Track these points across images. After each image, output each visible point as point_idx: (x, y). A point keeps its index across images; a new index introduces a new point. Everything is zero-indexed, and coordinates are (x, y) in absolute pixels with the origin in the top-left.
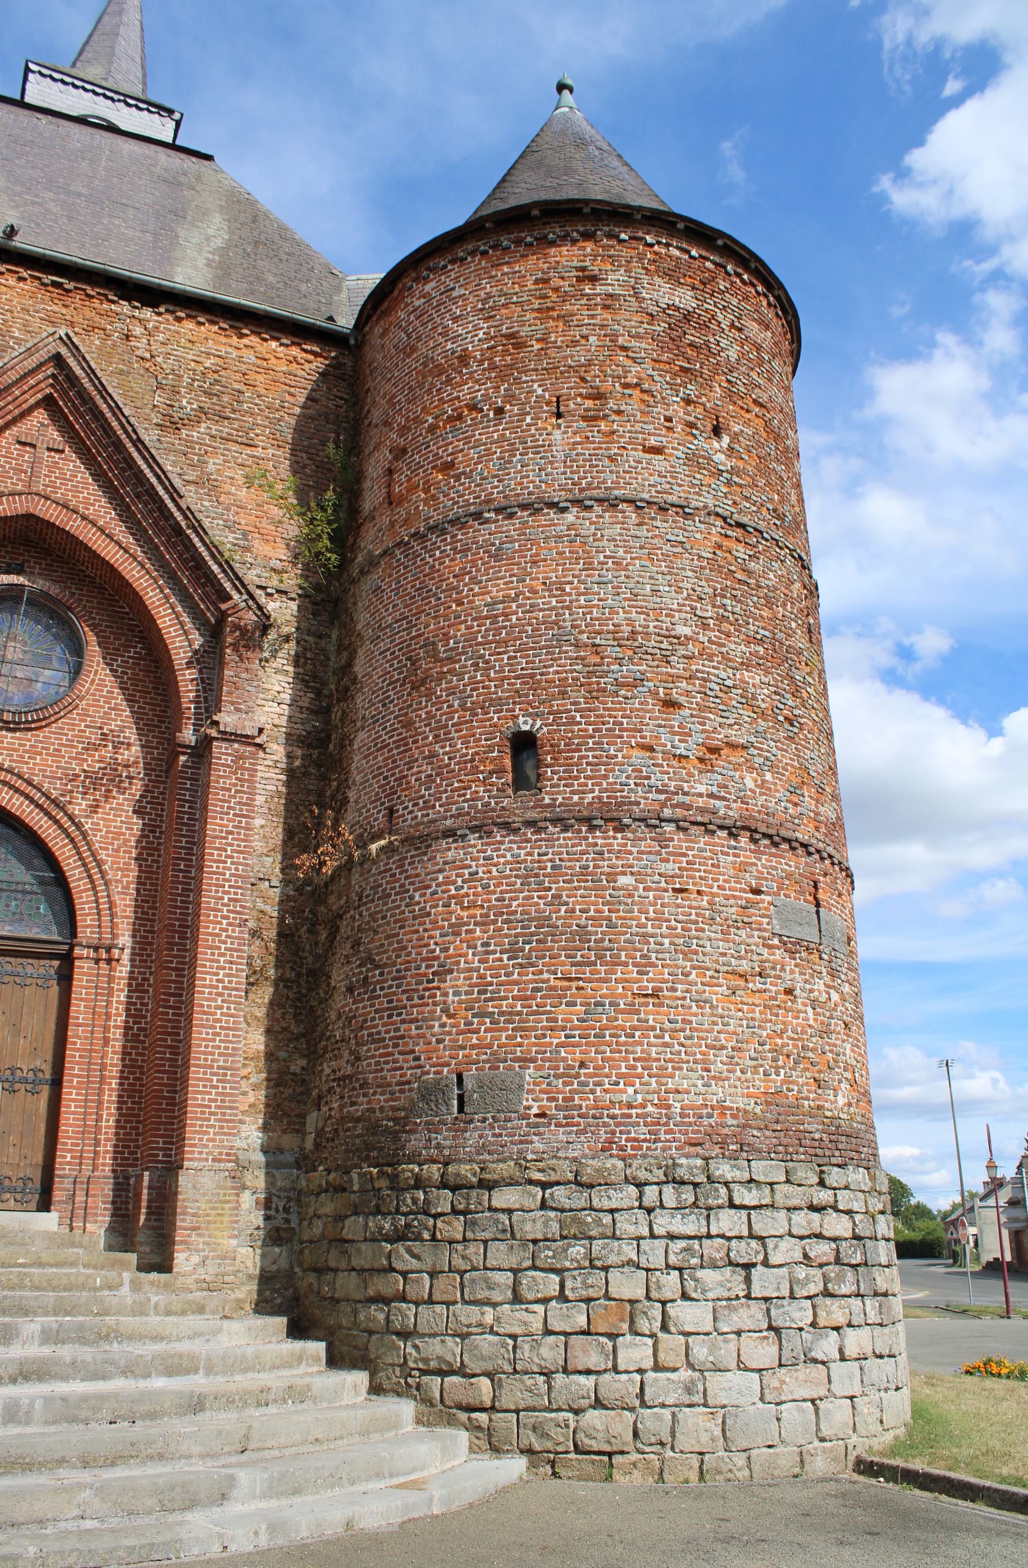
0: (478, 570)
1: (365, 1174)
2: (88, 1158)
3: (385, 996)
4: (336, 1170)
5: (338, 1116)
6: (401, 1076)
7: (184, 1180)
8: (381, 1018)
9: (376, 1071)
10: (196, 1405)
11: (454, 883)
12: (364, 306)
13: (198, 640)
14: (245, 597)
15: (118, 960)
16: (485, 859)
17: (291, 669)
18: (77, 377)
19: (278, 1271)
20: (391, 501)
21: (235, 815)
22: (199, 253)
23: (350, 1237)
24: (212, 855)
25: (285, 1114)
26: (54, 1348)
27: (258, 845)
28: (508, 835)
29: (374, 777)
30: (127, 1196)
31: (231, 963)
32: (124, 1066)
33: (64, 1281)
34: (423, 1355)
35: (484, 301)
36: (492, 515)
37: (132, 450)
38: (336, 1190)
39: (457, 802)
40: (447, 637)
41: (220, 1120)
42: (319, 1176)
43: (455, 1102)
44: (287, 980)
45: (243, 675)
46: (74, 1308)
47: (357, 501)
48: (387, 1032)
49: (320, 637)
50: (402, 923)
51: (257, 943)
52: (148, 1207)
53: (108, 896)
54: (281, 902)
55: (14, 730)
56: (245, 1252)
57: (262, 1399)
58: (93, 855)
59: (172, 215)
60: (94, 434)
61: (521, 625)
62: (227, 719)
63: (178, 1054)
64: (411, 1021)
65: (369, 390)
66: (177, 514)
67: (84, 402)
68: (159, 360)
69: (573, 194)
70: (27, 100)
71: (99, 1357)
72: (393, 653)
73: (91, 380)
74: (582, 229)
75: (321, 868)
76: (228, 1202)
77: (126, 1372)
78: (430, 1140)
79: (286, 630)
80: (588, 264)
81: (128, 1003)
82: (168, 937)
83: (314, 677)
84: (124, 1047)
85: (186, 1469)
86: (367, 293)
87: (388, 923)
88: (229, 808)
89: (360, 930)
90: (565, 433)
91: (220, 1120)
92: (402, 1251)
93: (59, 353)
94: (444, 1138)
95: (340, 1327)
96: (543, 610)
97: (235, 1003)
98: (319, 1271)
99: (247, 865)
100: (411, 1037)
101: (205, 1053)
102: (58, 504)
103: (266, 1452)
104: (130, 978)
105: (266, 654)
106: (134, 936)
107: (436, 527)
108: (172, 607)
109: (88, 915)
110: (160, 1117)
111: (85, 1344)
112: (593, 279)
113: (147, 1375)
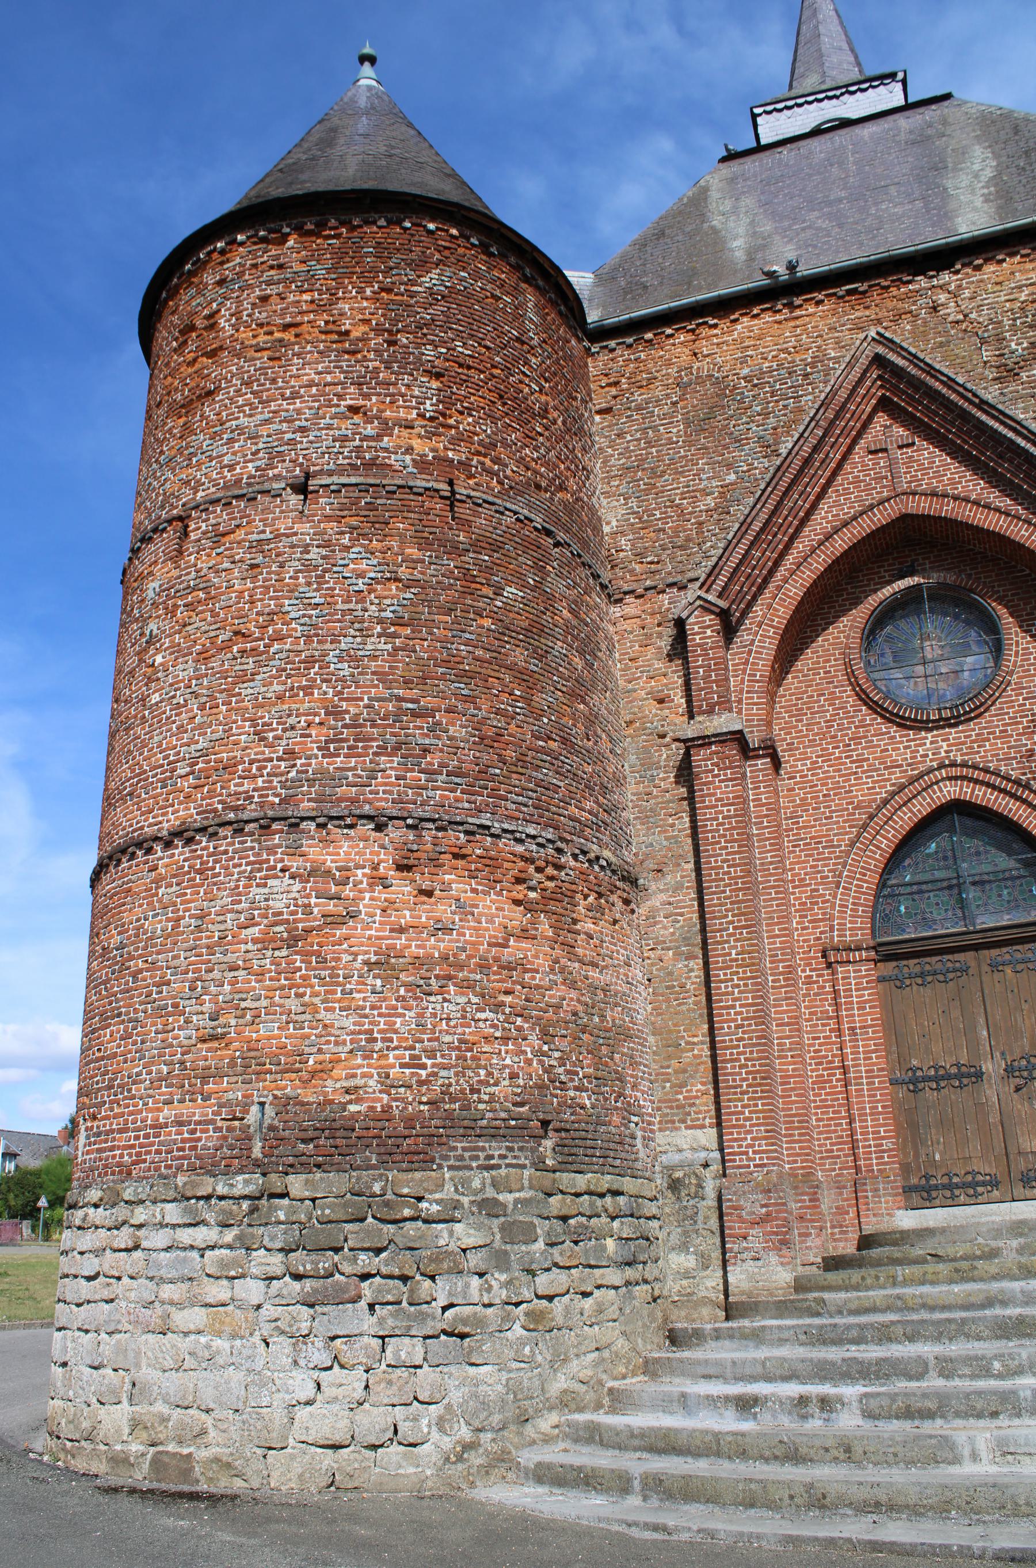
18: (902, 369)
22: (973, 192)
37: (979, 414)
55: (956, 725)
59: (933, 169)
60: (937, 414)
67: (917, 389)
68: (973, 316)
70: (763, 142)
73: (916, 365)
102: (926, 495)
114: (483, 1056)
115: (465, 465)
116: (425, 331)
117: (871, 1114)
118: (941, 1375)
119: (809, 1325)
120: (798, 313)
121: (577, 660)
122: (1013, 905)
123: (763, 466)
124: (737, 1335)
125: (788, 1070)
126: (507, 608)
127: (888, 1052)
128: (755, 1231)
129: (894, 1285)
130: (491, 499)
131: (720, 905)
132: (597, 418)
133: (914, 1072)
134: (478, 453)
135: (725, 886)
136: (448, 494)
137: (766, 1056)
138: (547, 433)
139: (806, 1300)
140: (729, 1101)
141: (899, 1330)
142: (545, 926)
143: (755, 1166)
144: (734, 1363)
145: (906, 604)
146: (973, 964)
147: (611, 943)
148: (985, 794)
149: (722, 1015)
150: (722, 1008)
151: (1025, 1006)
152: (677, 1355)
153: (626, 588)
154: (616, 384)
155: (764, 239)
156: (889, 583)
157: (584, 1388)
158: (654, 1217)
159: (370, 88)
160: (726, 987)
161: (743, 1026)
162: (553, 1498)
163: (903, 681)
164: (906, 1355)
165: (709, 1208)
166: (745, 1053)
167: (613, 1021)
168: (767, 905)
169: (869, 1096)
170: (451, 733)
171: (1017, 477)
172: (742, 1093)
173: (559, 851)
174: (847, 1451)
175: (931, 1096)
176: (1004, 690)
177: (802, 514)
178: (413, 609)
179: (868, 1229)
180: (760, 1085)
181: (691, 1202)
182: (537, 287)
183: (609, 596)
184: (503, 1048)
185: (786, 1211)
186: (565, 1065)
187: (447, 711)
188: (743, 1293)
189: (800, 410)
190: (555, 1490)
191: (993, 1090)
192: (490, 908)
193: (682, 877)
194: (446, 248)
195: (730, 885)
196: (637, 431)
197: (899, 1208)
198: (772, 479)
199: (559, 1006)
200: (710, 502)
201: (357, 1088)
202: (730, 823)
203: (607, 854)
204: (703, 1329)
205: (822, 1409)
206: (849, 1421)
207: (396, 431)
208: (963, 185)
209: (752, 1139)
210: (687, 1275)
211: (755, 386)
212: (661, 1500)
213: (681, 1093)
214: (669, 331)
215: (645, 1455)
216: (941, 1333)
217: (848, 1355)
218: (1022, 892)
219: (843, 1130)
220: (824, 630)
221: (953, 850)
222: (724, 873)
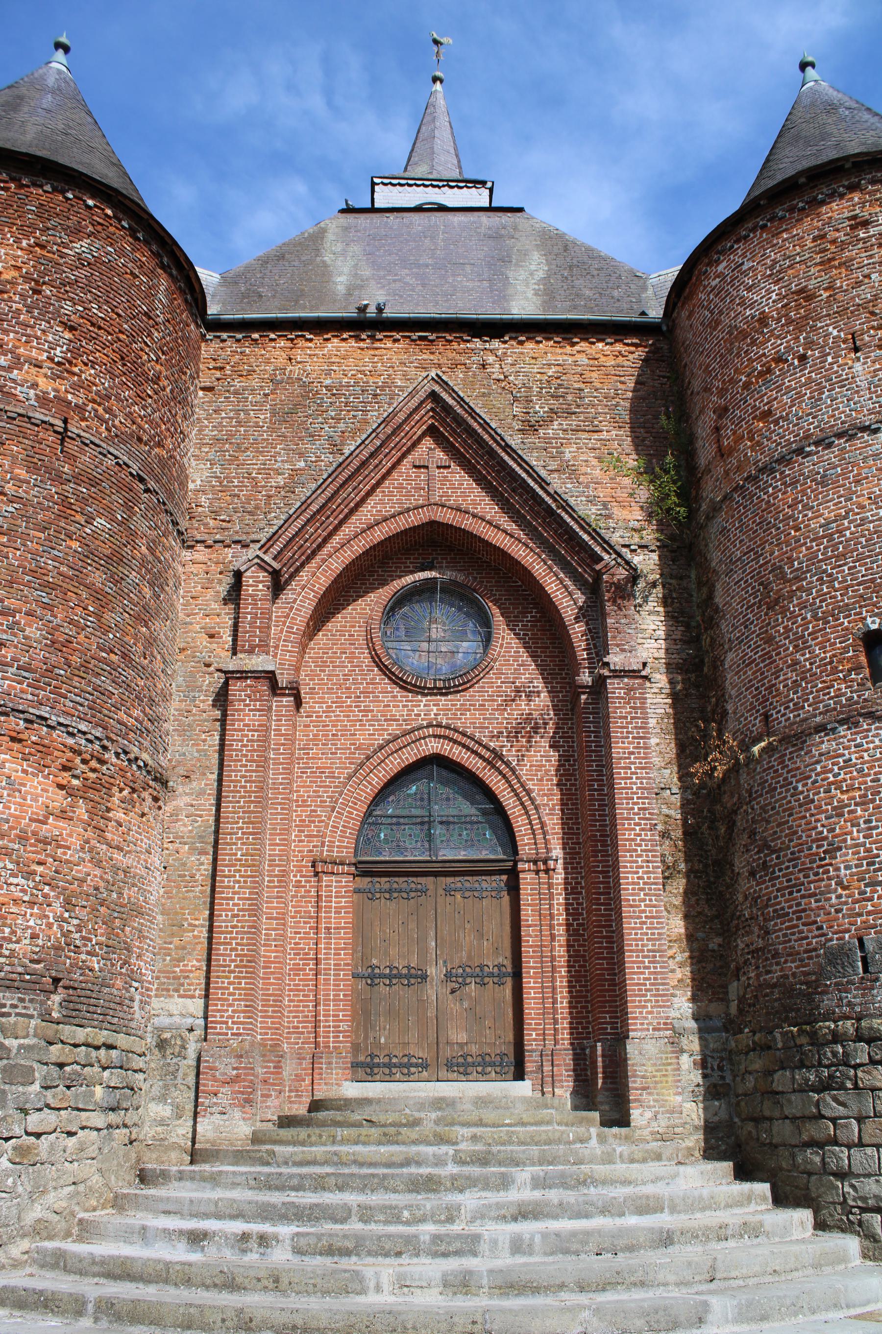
0: (809, 498)
1: (787, 1032)
2: (550, 1035)
3: (783, 876)
4: (760, 1031)
5: (756, 984)
6: (808, 944)
7: (631, 1048)
8: (783, 895)
9: (785, 942)
10: (666, 1239)
11: (831, 771)
12: (669, 297)
13: (581, 599)
14: (614, 556)
15: (554, 870)
16: (856, 746)
17: (661, 609)
19: (720, 1122)
20: (722, 453)
21: (634, 738)
22: (527, 286)
23: (780, 1089)
24: (620, 773)
25: (710, 986)
26: (543, 1192)
27: (656, 760)
28: (874, 723)
29: (746, 690)
30: (585, 1064)
31: (648, 862)
32: (569, 956)
33: (544, 1137)
34: (860, 1194)
35: (772, 268)
36: (813, 448)
37: (503, 454)
38: (762, 1049)
39: (823, 701)
40: (791, 560)
41: (655, 996)
42: (746, 1037)
43: (860, 964)
44: (697, 871)
45: (623, 621)
46: (555, 1158)
47: (693, 460)
48: (790, 907)
49: (681, 578)
50: (790, 811)
51: (667, 842)
52: (603, 1073)
53: (539, 818)
54: (683, 806)
55: (446, 694)
56: (690, 1106)
57: (721, 1234)
58: (522, 786)
59: (501, 261)
60: (471, 448)
61: (854, 538)
62: (615, 659)
63: (613, 942)
64: (810, 896)
65: (686, 364)
66: (547, 499)
67: (459, 425)
68: (511, 378)
69: (833, 154)
70: (377, 205)
71: (581, 1199)
72: (746, 581)
73: (462, 406)
74: (846, 183)
75: (713, 772)
76: (670, 1064)
77: (604, 1211)
78: (841, 999)
79: (652, 577)
80: (858, 211)
81: (566, 904)
82: (592, 846)
83: (682, 612)
84: (568, 941)
85: (665, 1295)
86: (669, 285)
87: (778, 813)
88: (628, 732)
89: (754, 821)
90: (864, 364)
91: (655, 996)
92: (828, 1099)
93: (433, 391)
94: (853, 996)
95: (781, 1169)
96: (873, 521)
97: (655, 895)
98: (757, 1120)
99: (650, 778)
100: (812, 910)
101: (636, 940)
103: (732, 1281)
104: (565, 883)
105: (639, 601)
106: (564, 849)
107: (765, 467)
108: (556, 575)
109: (525, 835)
110: (605, 996)
111: (567, 1188)
112: (865, 224)
113: (622, 1214)
114: (9, 916)
115: (80, 409)
116: (68, 288)
117: (334, 1000)
118: (361, 1220)
119: (259, 1173)
120: (378, 345)
121: (147, 590)
122: (470, 844)
123: (328, 461)
124: (198, 1177)
125: (270, 957)
126: (94, 536)
127: (355, 951)
128: (225, 1089)
129: (334, 1143)
130: (97, 441)
131: (234, 813)
132: (201, 393)
133: (373, 969)
134: (94, 401)
135: (240, 797)
136: (61, 430)
137: (253, 943)
138: (155, 397)
139: (259, 1151)
140: (218, 977)
141: (332, 1181)
142: (82, 810)
143: (232, 1034)
144: (191, 1201)
145: (422, 592)
146: (431, 887)
147: (137, 832)
148: (460, 752)
149: (222, 904)
150: (223, 898)
151: (467, 926)
152: (144, 1192)
153: (199, 538)
154: (221, 369)
155: (362, 281)
156: (412, 572)
157: (57, 1217)
158: (141, 1070)
159: (59, 72)
160: (229, 882)
161: (238, 916)
162: (13, 1320)
163: (410, 653)
164: (335, 1202)
165: (189, 1067)
166: (236, 938)
167: (129, 898)
168: (273, 818)
169: (334, 985)
170: (27, 633)
171: (524, 508)
172: (229, 972)
173: (105, 748)
174: (275, 1282)
175: (383, 990)
176: (488, 673)
177: (352, 505)
178: (12, 521)
179: (319, 1095)
180: (245, 966)
181: (174, 1060)
182: (171, 275)
183: (183, 542)
184: (29, 911)
185: (253, 1075)
186: (81, 931)
187: (27, 614)
188: (208, 1141)
189: (366, 422)
190: (16, 1313)
191: (434, 991)
192: (36, 788)
193: (206, 785)
194: (99, 224)
195: (244, 797)
196: (231, 410)
197: (346, 1080)
198: (333, 472)
199: (83, 881)
200: (281, 481)
202: (252, 746)
203: (145, 756)
204: (169, 1171)
205: (260, 1245)
206: (281, 1256)
207: (26, 366)
208: (521, 278)
209: (233, 1011)
210: (162, 1122)
211: (334, 395)
212: (110, 1322)
213: (179, 966)
214: (272, 336)
215: (102, 1280)
216: (365, 1185)
217: (288, 1199)
218: (478, 835)
219: (309, 1011)
220: (354, 601)
221: (429, 794)
222: (241, 787)
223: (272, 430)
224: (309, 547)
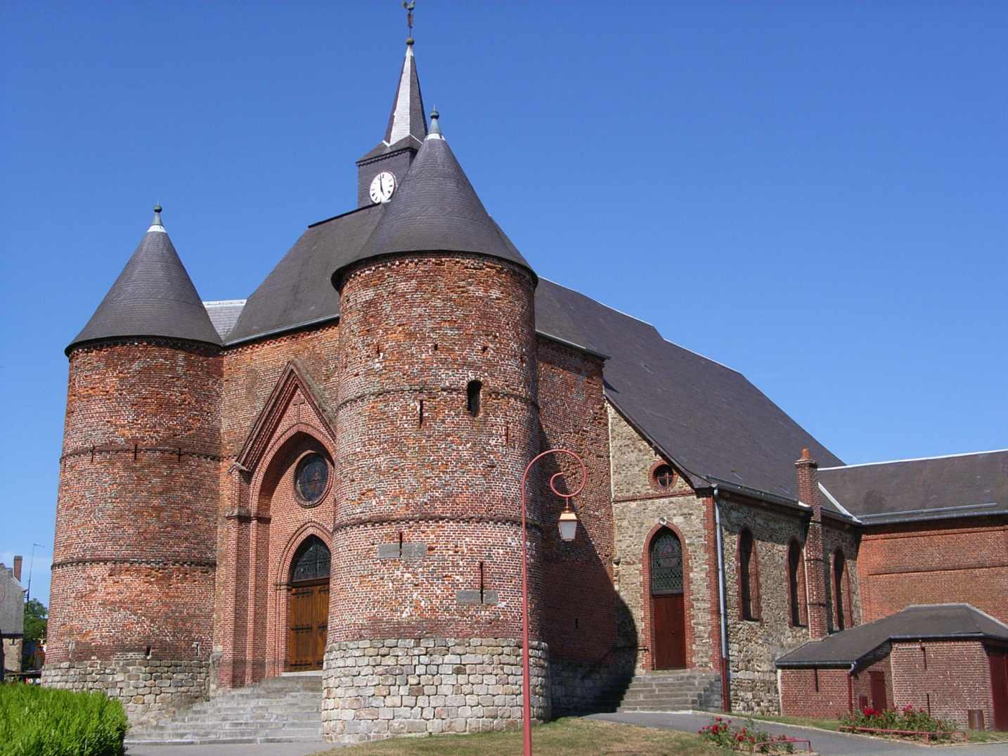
55: (314, 507)
201: (94, 639)
223: (246, 398)
224: (258, 453)
